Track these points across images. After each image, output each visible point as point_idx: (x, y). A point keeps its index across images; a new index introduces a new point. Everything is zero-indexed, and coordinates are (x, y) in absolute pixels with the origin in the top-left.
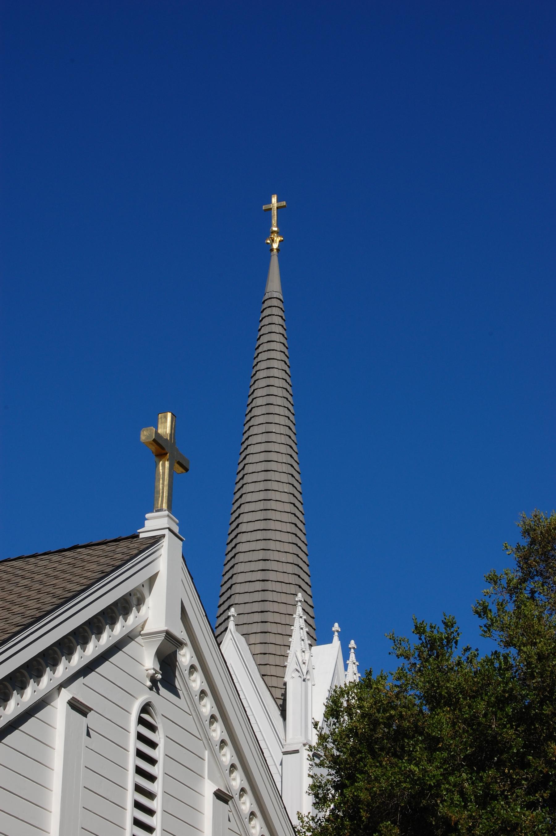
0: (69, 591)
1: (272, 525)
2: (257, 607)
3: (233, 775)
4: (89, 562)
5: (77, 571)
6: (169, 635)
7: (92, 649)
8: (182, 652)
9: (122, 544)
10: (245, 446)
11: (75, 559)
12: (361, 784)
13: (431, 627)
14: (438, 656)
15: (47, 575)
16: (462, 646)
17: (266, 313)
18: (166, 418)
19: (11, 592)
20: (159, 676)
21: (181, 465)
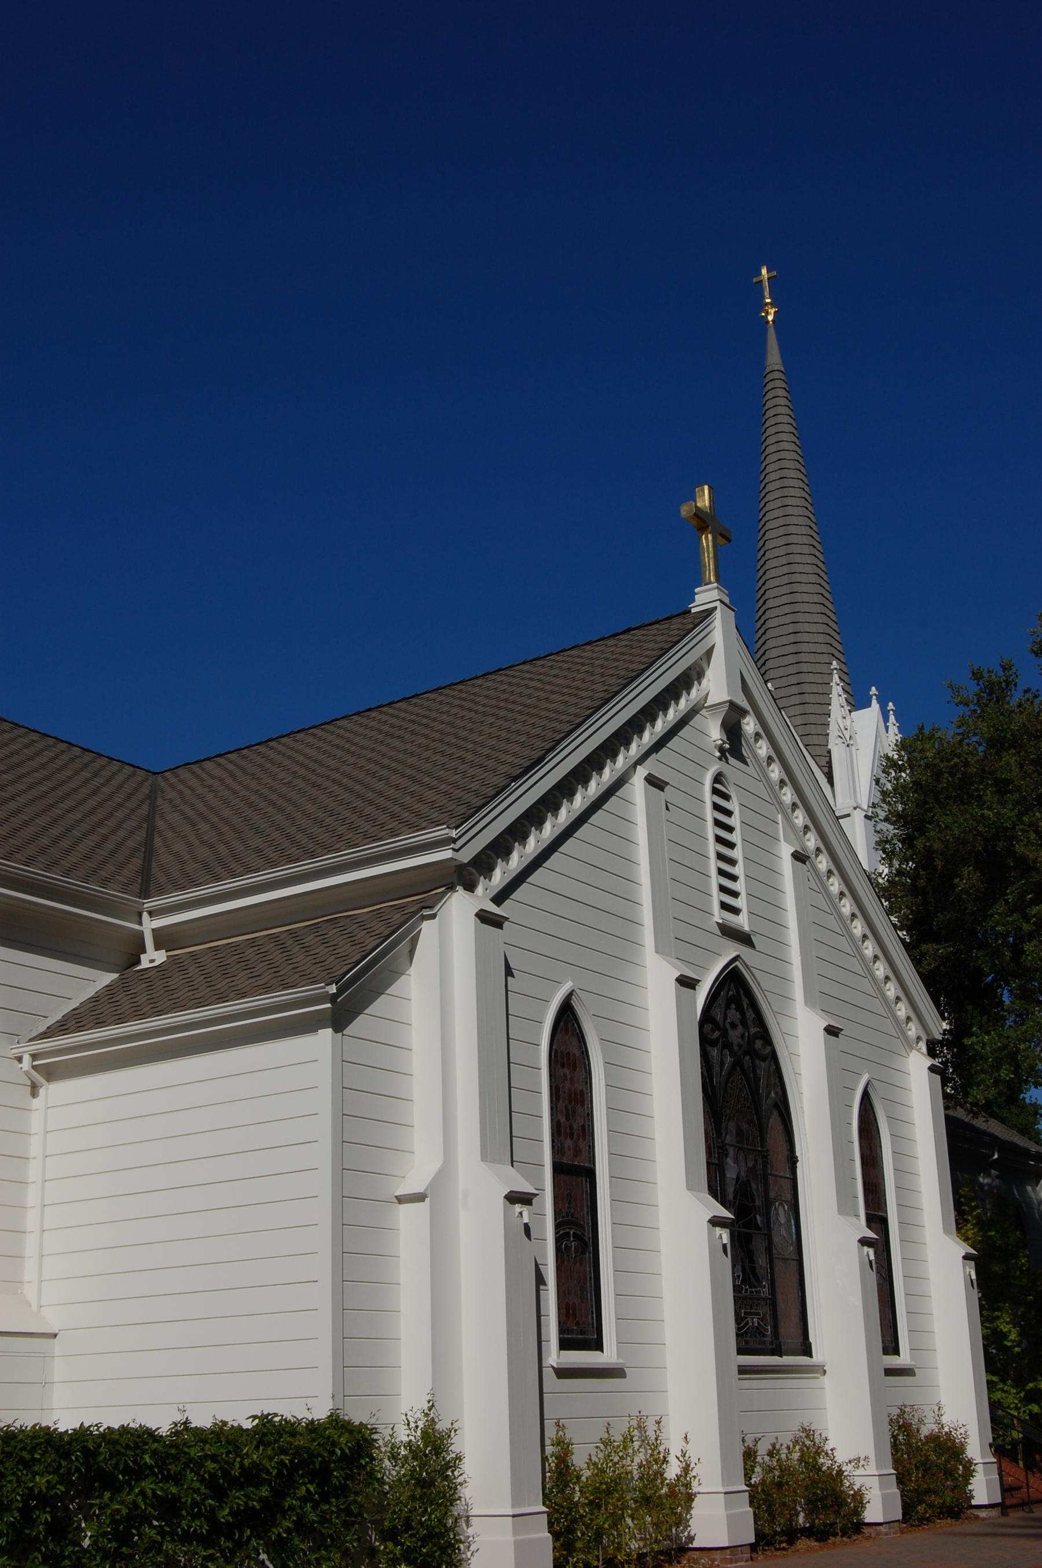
0: (633, 671)
1: (798, 597)
2: (793, 680)
3: (807, 836)
4: (645, 642)
5: (636, 651)
6: (732, 705)
7: (660, 726)
8: (746, 721)
9: (674, 621)
10: (762, 522)
11: (631, 640)
12: (932, 833)
13: (989, 672)
14: (998, 700)
15: (607, 659)
16: (1021, 688)
17: (768, 387)
18: (703, 491)
19: (574, 679)
20: (728, 746)
21: (723, 536)
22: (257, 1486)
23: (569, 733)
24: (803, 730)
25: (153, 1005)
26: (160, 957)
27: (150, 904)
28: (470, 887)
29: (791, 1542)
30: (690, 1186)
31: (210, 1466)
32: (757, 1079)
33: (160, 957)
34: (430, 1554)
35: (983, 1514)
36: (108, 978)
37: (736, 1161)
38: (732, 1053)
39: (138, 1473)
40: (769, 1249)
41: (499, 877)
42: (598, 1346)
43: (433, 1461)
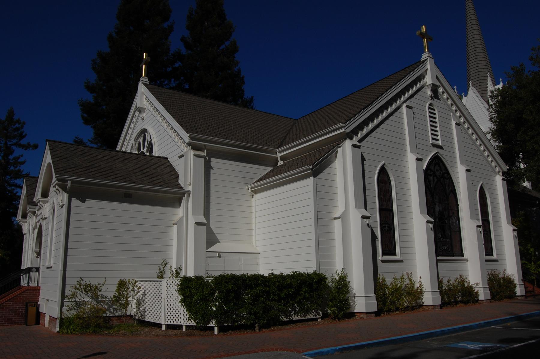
2: (477, 79)
23: (380, 96)
24: (481, 92)
25: (280, 173)
26: (282, 163)
27: (279, 150)
28: (351, 138)
29: (456, 305)
31: (277, 283)
33: (282, 163)
35: (519, 298)
37: (439, 206)
39: (257, 285)
41: (360, 135)
43: (343, 284)
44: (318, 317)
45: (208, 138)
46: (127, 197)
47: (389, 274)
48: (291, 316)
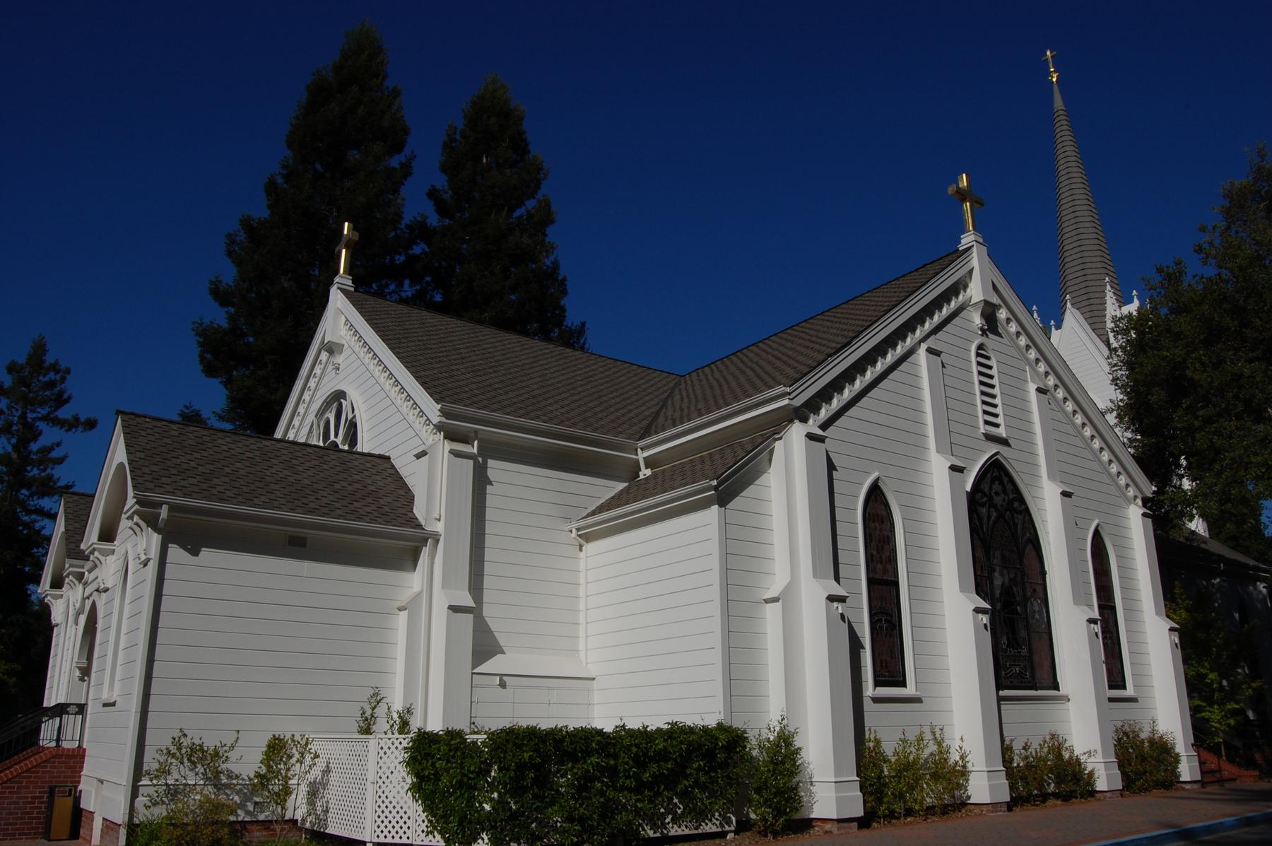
1: (1084, 242)
2: (1083, 291)
6: (986, 302)
21: (977, 203)
22: (666, 762)
25: (643, 497)
26: (648, 472)
27: (641, 443)
29: (1043, 802)
30: (962, 589)
31: (634, 749)
32: (1016, 526)
33: (648, 472)
34: (779, 803)
35: (1188, 787)
36: (623, 485)
37: (1002, 574)
38: (997, 510)
39: (588, 753)
40: (1027, 627)
41: (824, 413)
42: (1124, 688)
44: (727, 828)
45: (524, 421)
46: (295, 545)
47: (889, 728)
48: (664, 826)
